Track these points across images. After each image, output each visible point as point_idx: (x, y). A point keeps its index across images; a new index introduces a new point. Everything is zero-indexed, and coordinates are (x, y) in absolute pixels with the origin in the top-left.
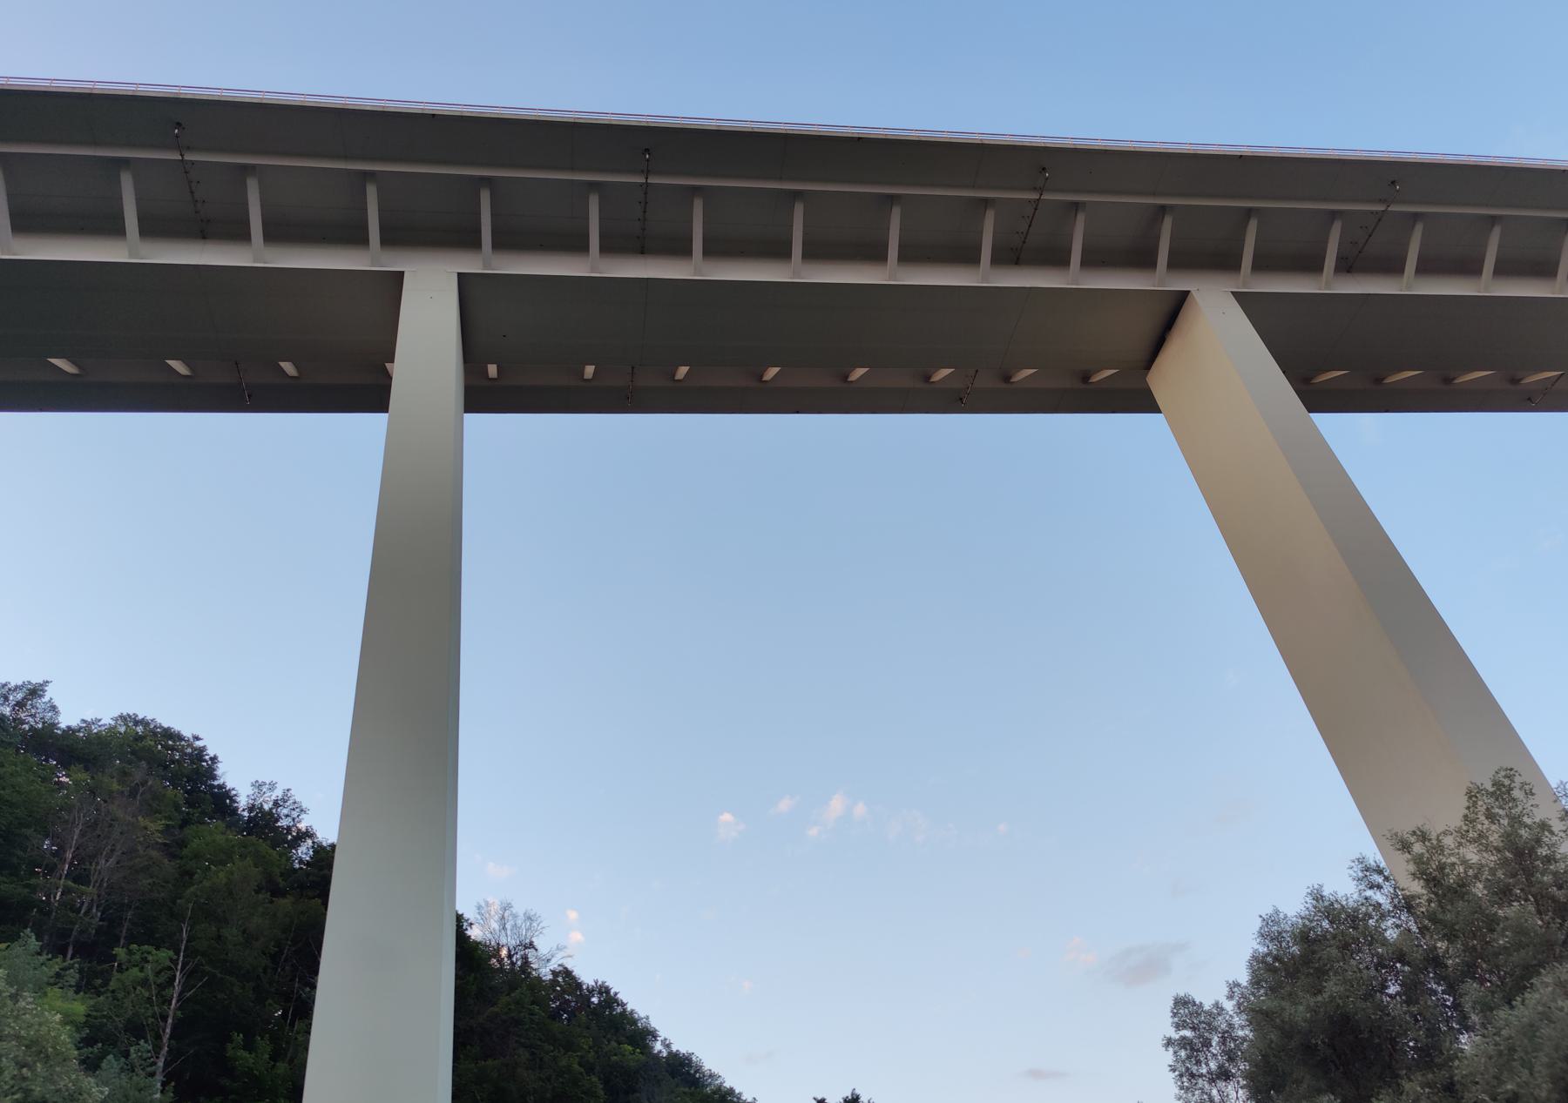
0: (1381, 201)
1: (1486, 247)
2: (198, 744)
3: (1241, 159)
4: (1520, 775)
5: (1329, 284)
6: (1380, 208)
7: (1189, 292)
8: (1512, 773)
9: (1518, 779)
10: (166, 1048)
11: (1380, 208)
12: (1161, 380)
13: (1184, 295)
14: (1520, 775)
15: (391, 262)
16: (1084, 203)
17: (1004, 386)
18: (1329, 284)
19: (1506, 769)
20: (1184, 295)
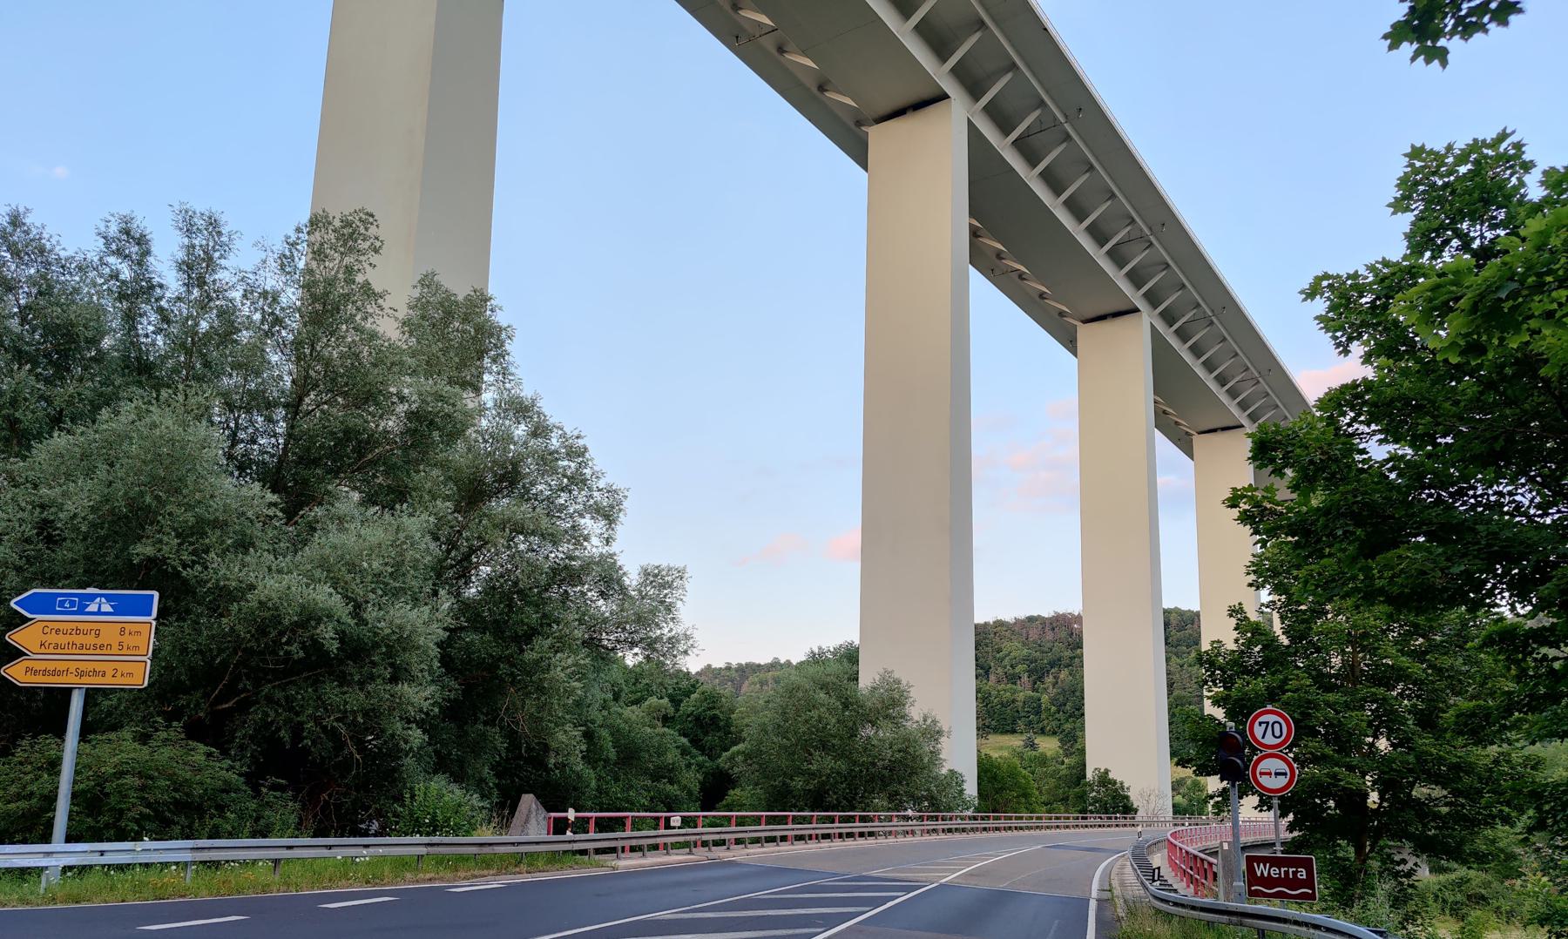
0: (1066, 116)
1: (1050, 152)
2: (581, 442)
3: (1210, 268)
4: (377, 226)
5: (1031, 179)
6: (1062, 120)
7: (948, 97)
8: (371, 220)
9: (373, 231)
10: (579, 768)
11: (1062, 120)
12: (879, 137)
13: (945, 97)
14: (377, 226)
15: (1140, 303)
16: (987, 27)
17: (853, 127)
18: (1031, 179)
19: (367, 214)
20: (945, 97)
